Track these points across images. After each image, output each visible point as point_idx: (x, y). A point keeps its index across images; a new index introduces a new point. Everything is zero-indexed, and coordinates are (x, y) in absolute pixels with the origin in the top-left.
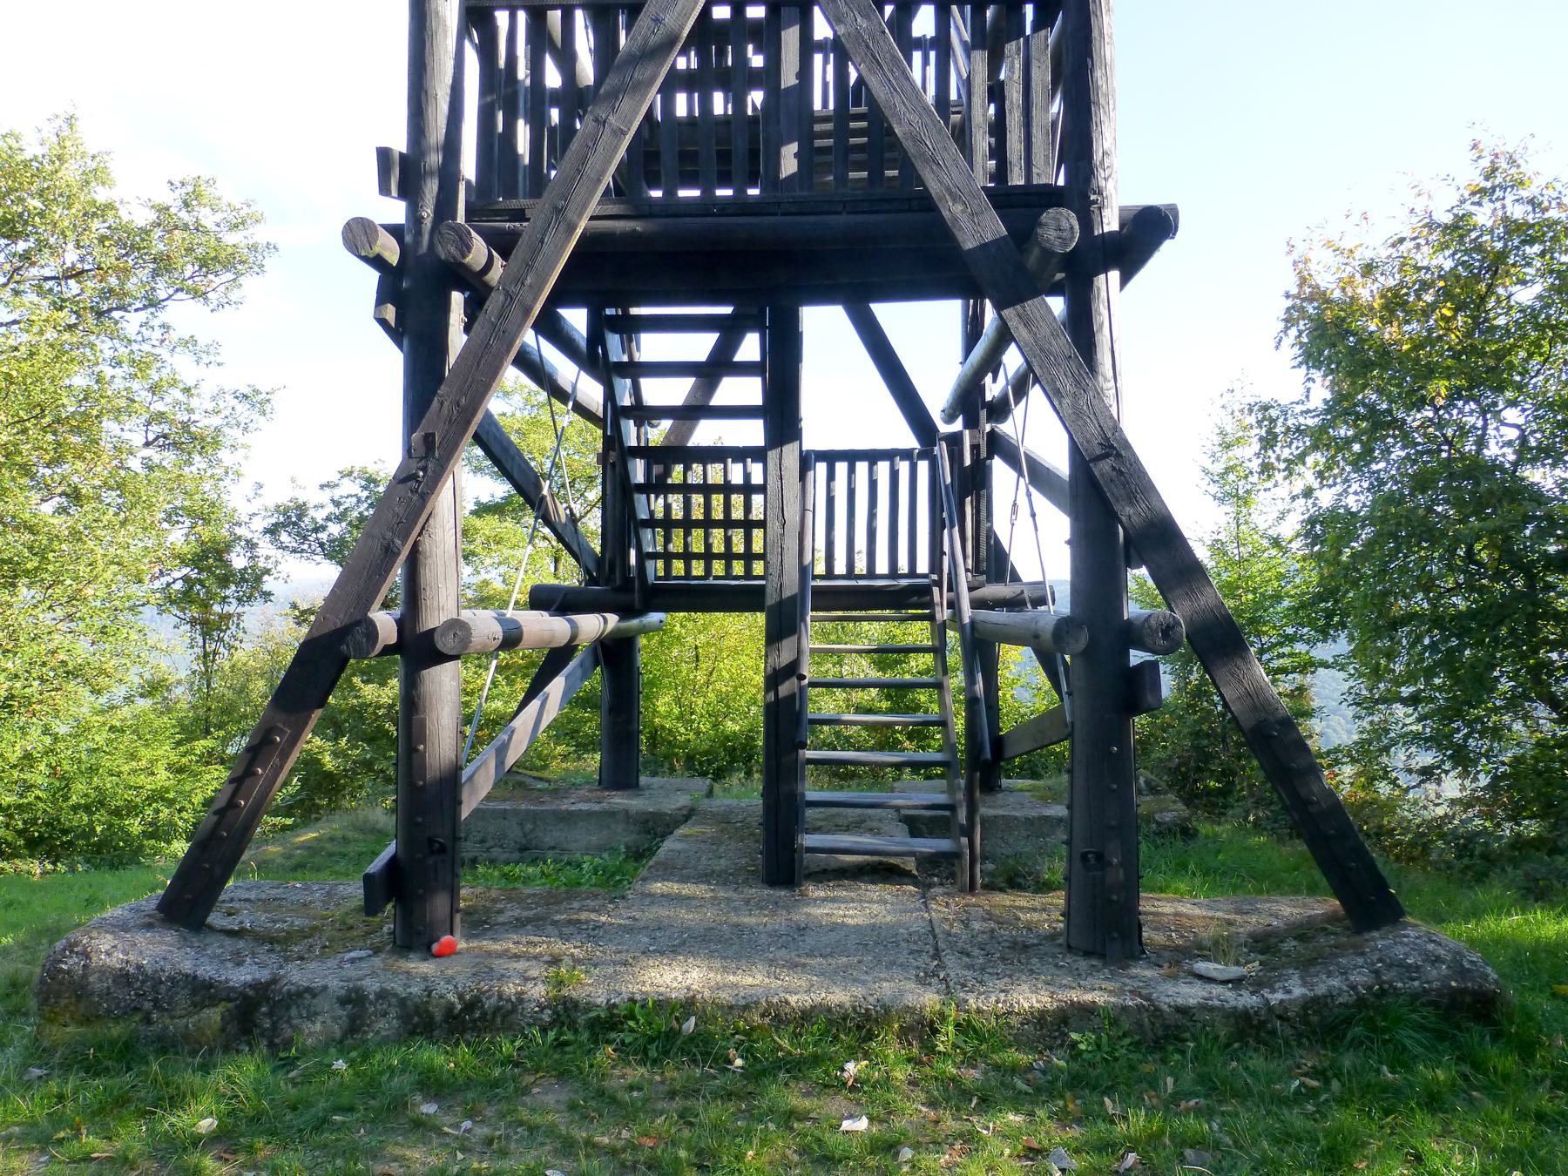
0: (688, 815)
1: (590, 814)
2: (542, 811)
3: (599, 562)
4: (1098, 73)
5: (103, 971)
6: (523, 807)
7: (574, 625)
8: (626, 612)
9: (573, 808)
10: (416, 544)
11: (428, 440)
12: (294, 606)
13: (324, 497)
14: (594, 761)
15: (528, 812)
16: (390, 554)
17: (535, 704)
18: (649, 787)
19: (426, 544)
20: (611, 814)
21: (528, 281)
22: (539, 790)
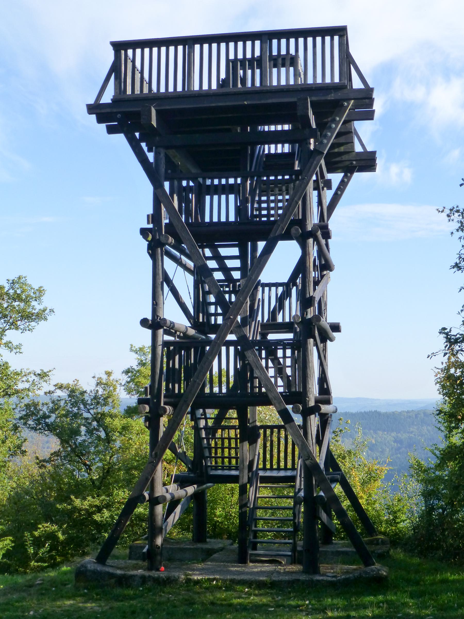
0: (222, 549)
1: (190, 549)
2: (175, 548)
3: (193, 463)
4: (308, 370)
5: (90, 571)
6: (168, 546)
7: (185, 490)
8: (200, 484)
9: (185, 547)
10: (153, 477)
11: (156, 454)
12: (37, 458)
13: (47, 399)
14: (190, 535)
15: (170, 548)
16: (147, 479)
17: (173, 515)
18: (210, 542)
19: (156, 477)
20: (197, 549)
21: (179, 418)
22: (172, 542)
